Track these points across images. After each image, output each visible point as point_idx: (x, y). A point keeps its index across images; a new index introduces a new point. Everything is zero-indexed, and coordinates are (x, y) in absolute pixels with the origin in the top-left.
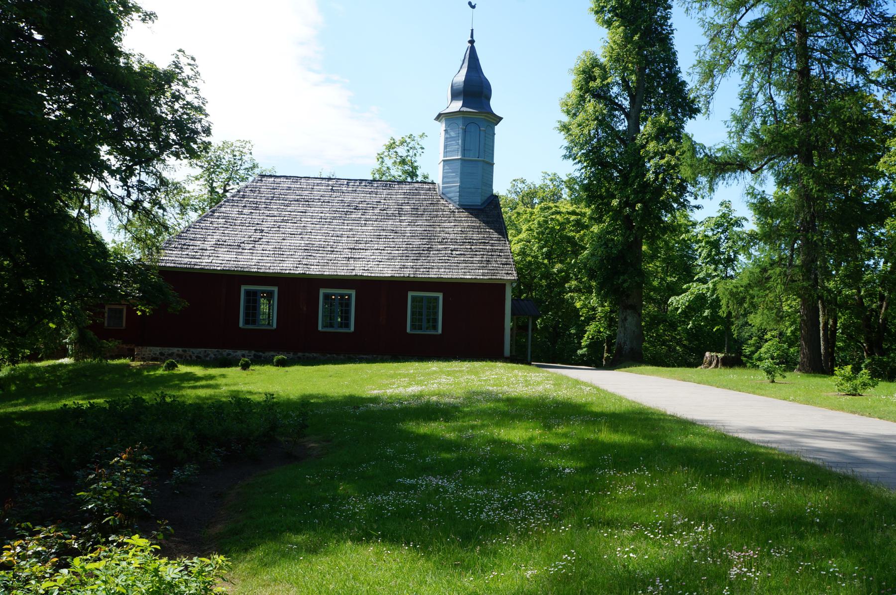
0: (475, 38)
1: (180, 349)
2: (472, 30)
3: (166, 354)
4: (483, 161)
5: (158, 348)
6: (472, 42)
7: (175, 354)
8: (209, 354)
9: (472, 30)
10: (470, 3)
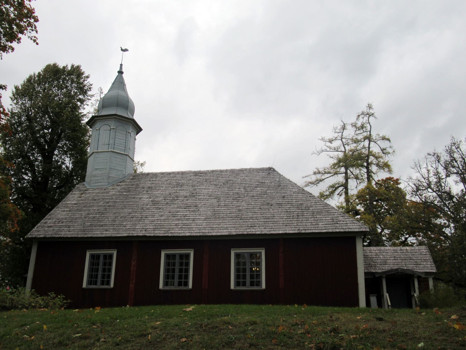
0: (123, 70)
2: (121, 65)
6: (121, 72)
9: (121, 65)
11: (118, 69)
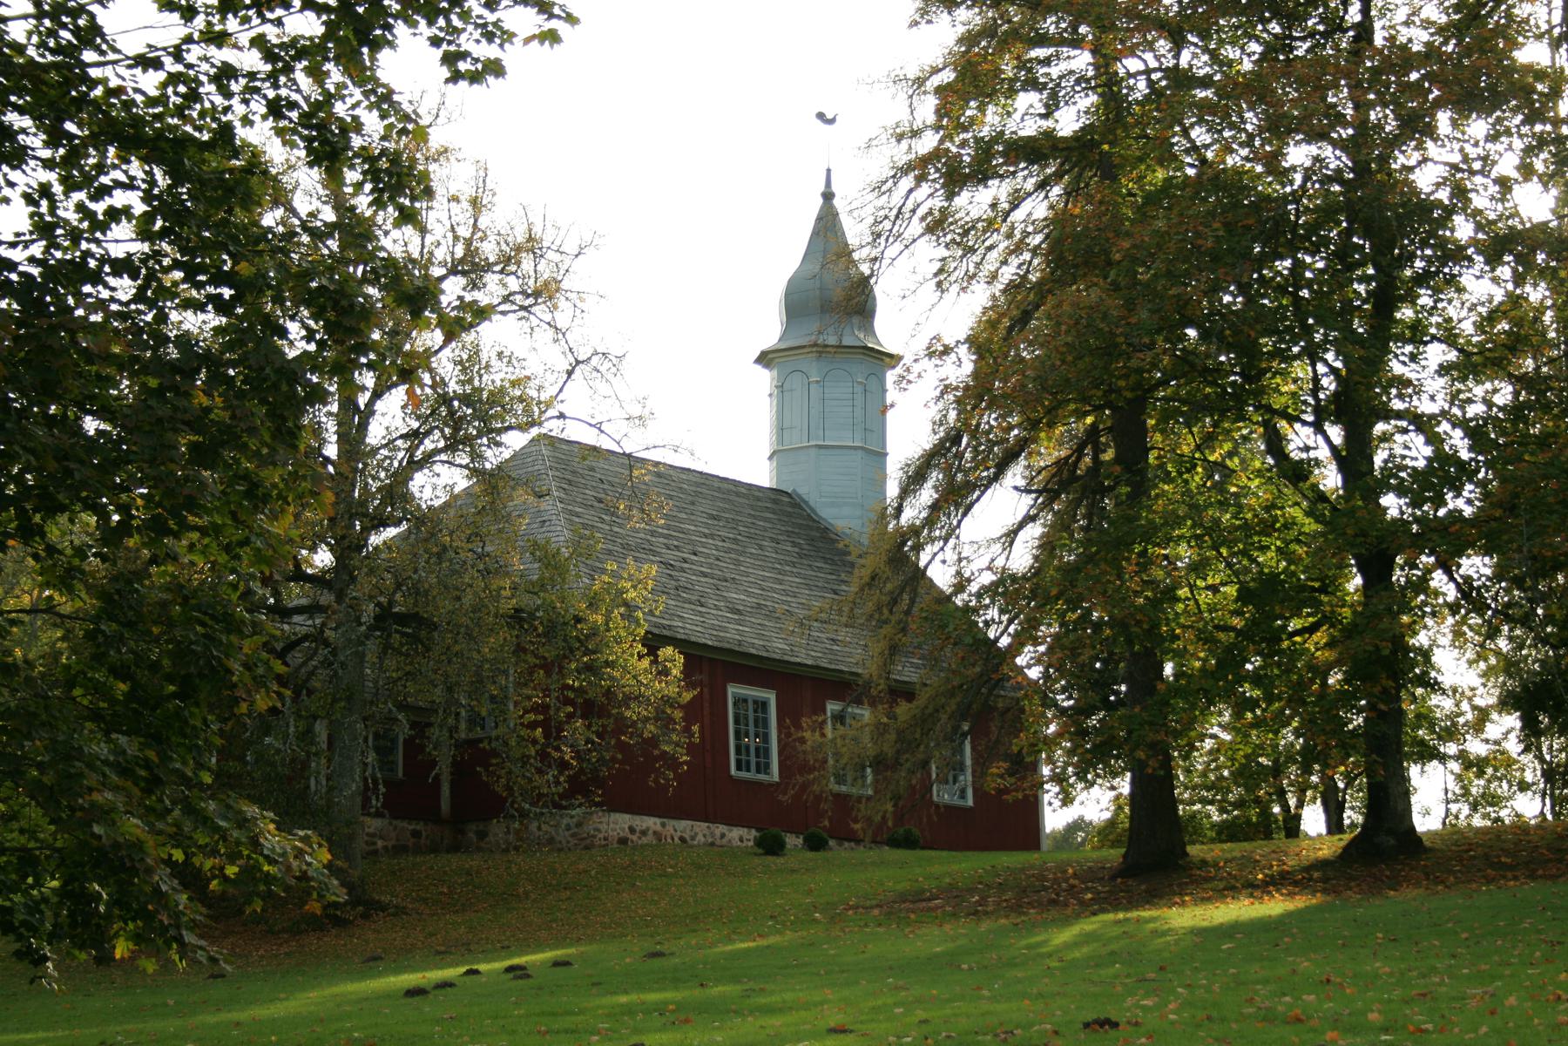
1: (658, 821)
2: (829, 171)
3: (638, 829)
4: (820, 447)
5: (627, 817)
6: (828, 196)
7: (651, 832)
8: (696, 834)
9: (829, 171)
10: (821, 116)
11: (822, 188)
